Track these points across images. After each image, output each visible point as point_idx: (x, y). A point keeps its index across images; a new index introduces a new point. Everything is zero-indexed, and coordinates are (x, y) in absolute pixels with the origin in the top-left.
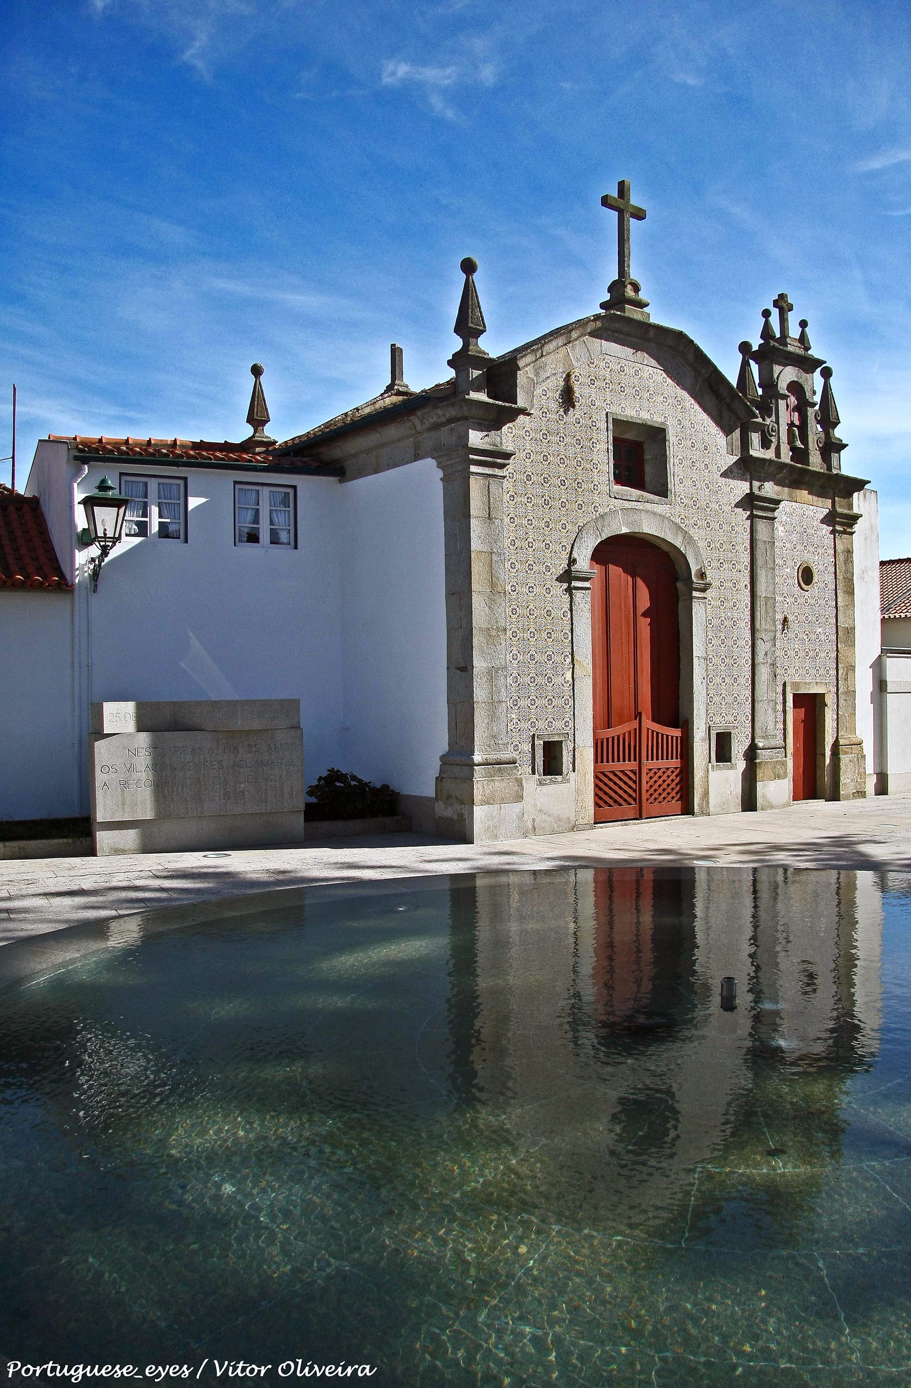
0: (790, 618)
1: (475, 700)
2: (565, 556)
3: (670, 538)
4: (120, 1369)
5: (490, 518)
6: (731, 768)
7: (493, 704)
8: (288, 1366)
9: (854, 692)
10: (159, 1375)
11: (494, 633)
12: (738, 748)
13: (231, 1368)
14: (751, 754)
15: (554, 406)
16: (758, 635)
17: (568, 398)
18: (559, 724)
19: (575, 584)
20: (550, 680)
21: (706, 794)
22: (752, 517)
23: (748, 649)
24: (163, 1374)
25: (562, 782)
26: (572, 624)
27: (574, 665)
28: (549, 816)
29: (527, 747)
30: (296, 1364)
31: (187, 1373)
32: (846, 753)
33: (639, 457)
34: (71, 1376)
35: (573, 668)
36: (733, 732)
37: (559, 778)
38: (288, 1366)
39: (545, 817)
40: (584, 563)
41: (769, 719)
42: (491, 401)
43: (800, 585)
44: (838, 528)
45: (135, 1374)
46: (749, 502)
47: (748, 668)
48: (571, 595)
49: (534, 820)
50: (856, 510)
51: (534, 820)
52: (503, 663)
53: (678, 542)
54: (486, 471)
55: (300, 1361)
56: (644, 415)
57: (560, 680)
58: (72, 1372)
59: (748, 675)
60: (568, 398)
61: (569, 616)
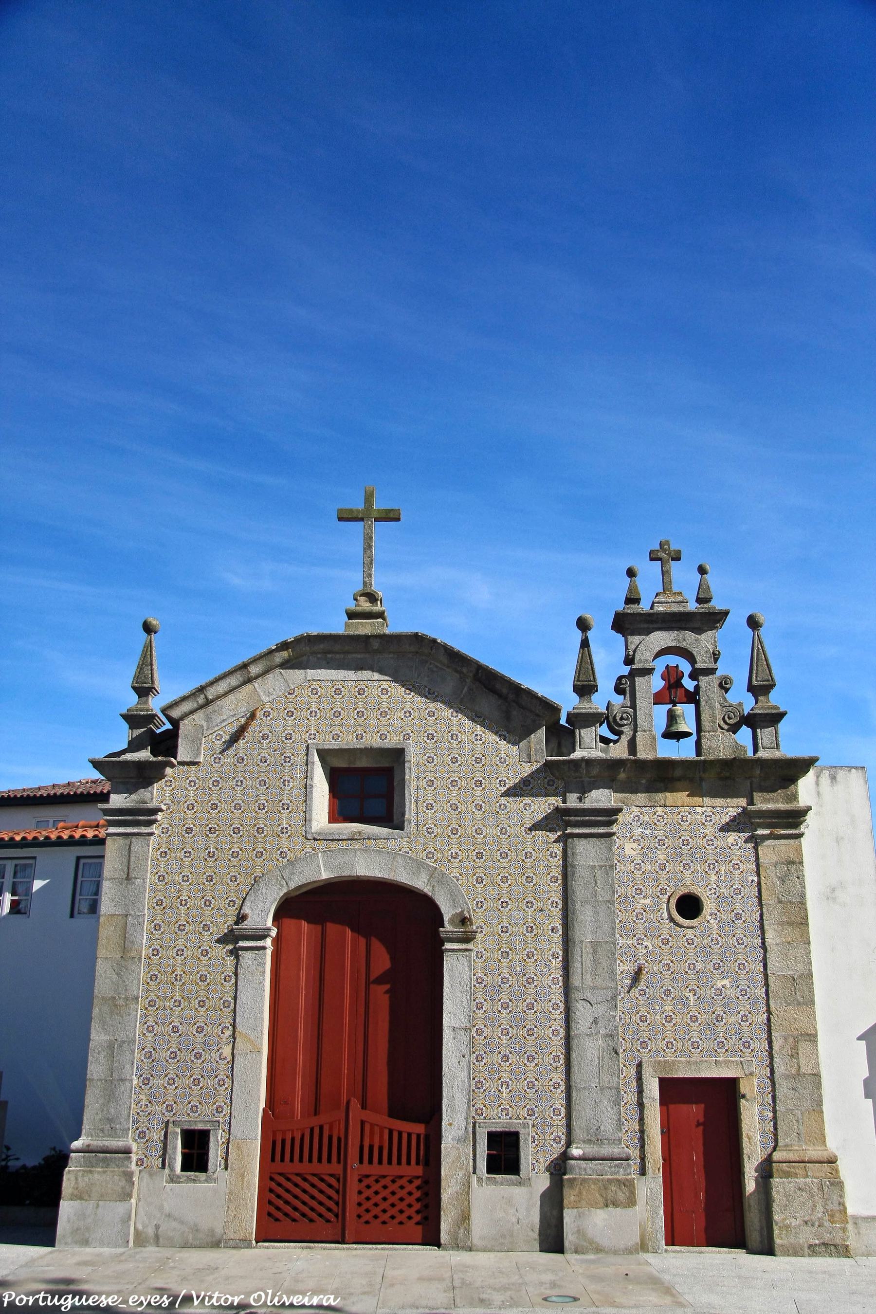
0: (651, 968)
1: (88, 1076)
2: (232, 912)
3: (403, 876)
4: (106, 1299)
5: (128, 878)
6: (520, 1184)
8: (260, 1296)
9: (817, 1075)
10: (141, 1303)
11: (121, 1002)
12: (534, 1158)
13: (207, 1298)
14: (559, 1168)
16: (576, 995)
18: (208, 1110)
19: (242, 944)
21: (465, 1218)
22: (564, 839)
23: (558, 1015)
24: (145, 1304)
25: (206, 1181)
26: (236, 990)
27: (235, 1038)
28: (182, 1223)
29: (157, 1136)
30: (267, 1295)
31: (167, 1302)
32: (787, 1175)
33: (368, 787)
34: (61, 1305)
35: (234, 1043)
36: (522, 1131)
37: (202, 1176)
38: (260, 1296)
39: (174, 1224)
40: (262, 914)
42: (155, 759)
43: (672, 920)
44: (760, 832)
45: (120, 1303)
46: (559, 821)
48: (237, 957)
49: (157, 1227)
51: (157, 1227)
52: (131, 1036)
53: (420, 883)
54: (121, 830)
55: (270, 1292)
56: (373, 737)
58: (62, 1301)
59: (558, 1050)
61: (233, 981)
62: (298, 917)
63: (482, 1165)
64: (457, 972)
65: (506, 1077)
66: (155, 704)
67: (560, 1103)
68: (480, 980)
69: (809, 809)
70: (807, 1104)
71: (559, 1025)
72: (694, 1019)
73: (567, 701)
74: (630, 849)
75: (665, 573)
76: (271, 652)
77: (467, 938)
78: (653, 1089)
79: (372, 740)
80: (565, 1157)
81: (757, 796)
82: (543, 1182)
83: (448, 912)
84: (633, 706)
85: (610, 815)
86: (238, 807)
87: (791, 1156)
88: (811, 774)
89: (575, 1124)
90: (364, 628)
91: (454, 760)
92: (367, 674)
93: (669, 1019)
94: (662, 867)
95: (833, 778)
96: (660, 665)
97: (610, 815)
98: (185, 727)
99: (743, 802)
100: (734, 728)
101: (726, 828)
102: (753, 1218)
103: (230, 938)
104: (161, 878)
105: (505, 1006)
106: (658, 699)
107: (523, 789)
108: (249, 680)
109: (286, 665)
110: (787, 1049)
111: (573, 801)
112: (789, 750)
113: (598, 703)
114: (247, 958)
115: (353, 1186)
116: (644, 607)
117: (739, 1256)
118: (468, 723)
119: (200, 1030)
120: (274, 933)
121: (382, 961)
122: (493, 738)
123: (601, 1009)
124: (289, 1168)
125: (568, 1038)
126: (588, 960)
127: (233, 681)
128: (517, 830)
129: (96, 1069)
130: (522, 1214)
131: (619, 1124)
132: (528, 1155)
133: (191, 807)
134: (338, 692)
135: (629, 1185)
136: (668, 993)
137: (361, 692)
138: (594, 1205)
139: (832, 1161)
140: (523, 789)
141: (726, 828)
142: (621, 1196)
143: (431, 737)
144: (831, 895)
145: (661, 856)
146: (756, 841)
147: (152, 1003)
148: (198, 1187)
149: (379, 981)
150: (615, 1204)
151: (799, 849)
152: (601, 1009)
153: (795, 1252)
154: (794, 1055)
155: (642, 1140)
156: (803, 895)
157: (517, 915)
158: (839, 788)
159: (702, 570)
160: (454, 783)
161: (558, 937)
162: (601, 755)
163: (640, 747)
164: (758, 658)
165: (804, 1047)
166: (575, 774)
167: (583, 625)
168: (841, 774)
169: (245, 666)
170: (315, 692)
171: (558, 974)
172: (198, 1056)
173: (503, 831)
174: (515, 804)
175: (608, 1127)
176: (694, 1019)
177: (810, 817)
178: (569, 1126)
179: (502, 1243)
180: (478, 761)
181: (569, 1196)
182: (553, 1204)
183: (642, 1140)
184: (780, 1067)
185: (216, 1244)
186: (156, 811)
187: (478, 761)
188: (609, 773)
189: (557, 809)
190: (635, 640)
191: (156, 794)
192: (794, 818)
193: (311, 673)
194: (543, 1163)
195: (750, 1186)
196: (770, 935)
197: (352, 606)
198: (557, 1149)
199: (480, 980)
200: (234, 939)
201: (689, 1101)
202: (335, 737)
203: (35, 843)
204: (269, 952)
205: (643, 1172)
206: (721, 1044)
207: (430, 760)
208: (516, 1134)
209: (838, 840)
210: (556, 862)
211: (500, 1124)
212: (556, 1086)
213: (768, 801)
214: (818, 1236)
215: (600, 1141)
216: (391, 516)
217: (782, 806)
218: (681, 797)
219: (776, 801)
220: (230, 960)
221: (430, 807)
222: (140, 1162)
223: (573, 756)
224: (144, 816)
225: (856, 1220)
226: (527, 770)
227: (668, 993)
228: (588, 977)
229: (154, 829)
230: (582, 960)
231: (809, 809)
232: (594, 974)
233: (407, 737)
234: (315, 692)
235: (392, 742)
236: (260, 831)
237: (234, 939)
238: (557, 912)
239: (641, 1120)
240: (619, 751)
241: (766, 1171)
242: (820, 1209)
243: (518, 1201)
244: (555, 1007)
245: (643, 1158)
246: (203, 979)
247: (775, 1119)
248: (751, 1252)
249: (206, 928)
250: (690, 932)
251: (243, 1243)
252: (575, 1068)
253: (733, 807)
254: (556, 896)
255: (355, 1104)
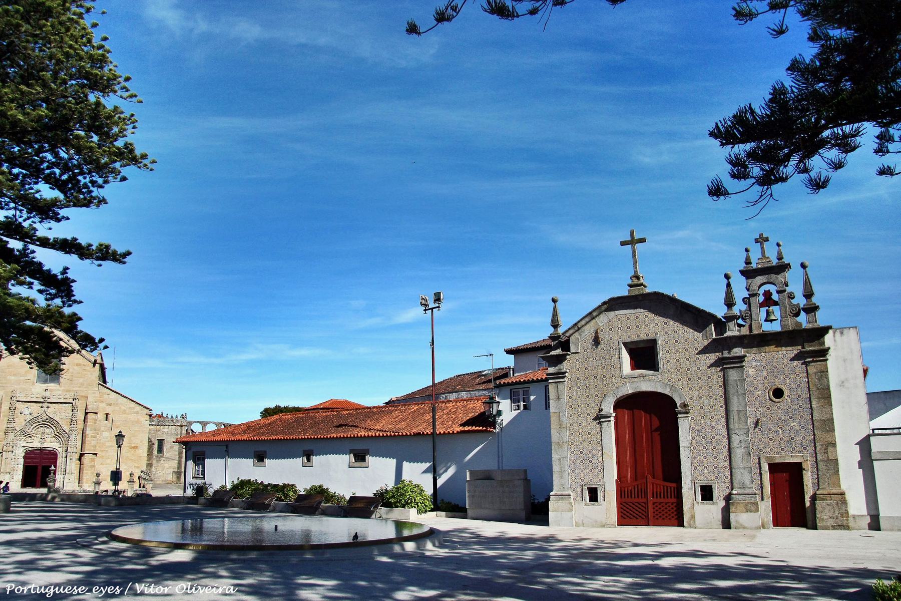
2: (597, 408)
3: (660, 390)
7: (561, 472)
9: (837, 460)
12: (719, 495)
14: (728, 498)
15: (590, 346)
17: (596, 341)
20: (590, 461)
21: (693, 517)
22: (723, 370)
23: (725, 440)
29: (579, 490)
32: (823, 499)
33: (644, 355)
40: (609, 408)
41: (744, 477)
43: (770, 399)
47: (726, 451)
50: (827, 345)
53: (667, 392)
56: (643, 335)
57: (596, 461)
59: (726, 454)
60: (596, 341)
62: (623, 408)
63: (699, 498)
64: (684, 426)
65: (706, 465)
66: (561, 331)
67: (728, 473)
68: (693, 428)
69: (829, 348)
70: (832, 472)
71: (725, 443)
72: (782, 439)
73: (720, 311)
74: (751, 371)
75: (762, 248)
76: (600, 306)
77: (687, 412)
78: (765, 467)
79: (643, 337)
80: (730, 494)
81: (806, 345)
82: (722, 504)
83: (678, 403)
84: (750, 310)
85: (741, 359)
86: (595, 368)
87: (824, 492)
88: (831, 331)
89: (734, 482)
90: (636, 291)
91: (676, 341)
92: (638, 310)
93: (771, 440)
94: (766, 378)
95: (842, 333)
96: (761, 291)
97: (741, 359)
98: (572, 339)
99: (800, 347)
100: (797, 314)
101: (792, 359)
102: (809, 516)
103: (597, 418)
104: (570, 397)
105: (704, 438)
106: (762, 305)
107: (705, 351)
108: (594, 318)
109: (607, 310)
110: (823, 450)
111: (726, 354)
112: (821, 322)
113: (736, 311)
114: (604, 425)
115: (650, 506)
116: (754, 266)
117: (803, 530)
118: (680, 325)
119: (590, 452)
120: (614, 415)
121: (656, 423)
122: (691, 330)
123: (742, 437)
124: (627, 500)
125: (730, 449)
126: (736, 418)
127: (587, 319)
128: (704, 368)
129: (555, 467)
130: (715, 515)
131: (752, 482)
132: (715, 493)
133: (578, 370)
134: (628, 318)
135: (756, 504)
136: (770, 429)
137: (637, 317)
138: (742, 512)
139: (843, 494)
140: (705, 351)
141: (792, 359)
142: (753, 508)
143: (666, 333)
144: (842, 384)
145: (765, 373)
146: (806, 364)
147: (572, 443)
148: (594, 507)
149: (656, 430)
150: (751, 511)
151: (826, 366)
152: (742, 437)
153: (826, 528)
154: (826, 452)
155: (762, 487)
156: (829, 385)
157: (706, 402)
158: (845, 337)
159: (778, 245)
160: (677, 351)
161: (723, 409)
162: (737, 333)
163: (754, 328)
164: (807, 285)
165: (830, 449)
166: (727, 343)
167: (727, 277)
168: (845, 331)
169: (590, 313)
170: (619, 319)
171: (724, 424)
172: (590, 461)
173: (698, 369)
174: (702, 357)
175: (747, 482)
176: (782, 439)
177: (830, 352)
178: (732, 483)
179: (708, 526)
180: (686, 341)
181: (732, 508)
182: (726, 512)
183: (762, 487)
184: (820, 457)
185: (604, 526)
186: (565, 372)
187: (686, 341)
188: (740, 341)
189: (719, 358)
190: (750, 281)
191: (565, 366)
192: (824, 352)
193: (617, 312)
194: (722, 498)
195: (808, 504)
196: (814, 404)
197: (630, 282)
198: (728, 491)
199: (693, 428)
200: (599, 418)
201: (782, 472)
202: (629, 337)
203: (529, 382)
204: (613, 423)
205: (762, 499)
206: (794, 449)
207: (667, 343)
208: (711, 486)
209: (845, 360)
210: (721, 379)
211: (705, 482)
212: (726, 467)
213: (810, 346)
214: (835, 522)
215: (744, 488)
216: (642, 240)
217: (816, 348)
218: (773, 348)
219: (814, 346)
220: (598, 426)
221: (668, 361)
222: (574, 499)
223: (725, 335)
224: (561, 375)
225: (854, 517)
226: (706, 342)
227: (770, 429)
228: (736, 425)
229: (566, 379)
230: (734, 418)
231: (829, 348)
232: (739, 423)
233: (657, 334)
234: (619, 319)
235: (651, 337)
236: (604, 376)
237: (599, 418)
238: (722, 399)
239: (761, 480)
240: (745, 331)
241: (814, 498)
242: (837, 512)
243: (714, 510)
244: (724, 437)
245: (762, 494)
246: (589, 433)
247: (818, 478)
248: (808, 528)
249: (588, 415)
250: (779, 405)
251: (612, 526)
252: (733, 460)
253: (794, 351)
254: (722, 393)
255: (649, 477)
